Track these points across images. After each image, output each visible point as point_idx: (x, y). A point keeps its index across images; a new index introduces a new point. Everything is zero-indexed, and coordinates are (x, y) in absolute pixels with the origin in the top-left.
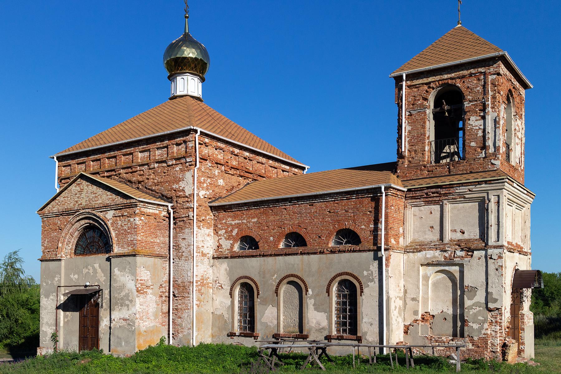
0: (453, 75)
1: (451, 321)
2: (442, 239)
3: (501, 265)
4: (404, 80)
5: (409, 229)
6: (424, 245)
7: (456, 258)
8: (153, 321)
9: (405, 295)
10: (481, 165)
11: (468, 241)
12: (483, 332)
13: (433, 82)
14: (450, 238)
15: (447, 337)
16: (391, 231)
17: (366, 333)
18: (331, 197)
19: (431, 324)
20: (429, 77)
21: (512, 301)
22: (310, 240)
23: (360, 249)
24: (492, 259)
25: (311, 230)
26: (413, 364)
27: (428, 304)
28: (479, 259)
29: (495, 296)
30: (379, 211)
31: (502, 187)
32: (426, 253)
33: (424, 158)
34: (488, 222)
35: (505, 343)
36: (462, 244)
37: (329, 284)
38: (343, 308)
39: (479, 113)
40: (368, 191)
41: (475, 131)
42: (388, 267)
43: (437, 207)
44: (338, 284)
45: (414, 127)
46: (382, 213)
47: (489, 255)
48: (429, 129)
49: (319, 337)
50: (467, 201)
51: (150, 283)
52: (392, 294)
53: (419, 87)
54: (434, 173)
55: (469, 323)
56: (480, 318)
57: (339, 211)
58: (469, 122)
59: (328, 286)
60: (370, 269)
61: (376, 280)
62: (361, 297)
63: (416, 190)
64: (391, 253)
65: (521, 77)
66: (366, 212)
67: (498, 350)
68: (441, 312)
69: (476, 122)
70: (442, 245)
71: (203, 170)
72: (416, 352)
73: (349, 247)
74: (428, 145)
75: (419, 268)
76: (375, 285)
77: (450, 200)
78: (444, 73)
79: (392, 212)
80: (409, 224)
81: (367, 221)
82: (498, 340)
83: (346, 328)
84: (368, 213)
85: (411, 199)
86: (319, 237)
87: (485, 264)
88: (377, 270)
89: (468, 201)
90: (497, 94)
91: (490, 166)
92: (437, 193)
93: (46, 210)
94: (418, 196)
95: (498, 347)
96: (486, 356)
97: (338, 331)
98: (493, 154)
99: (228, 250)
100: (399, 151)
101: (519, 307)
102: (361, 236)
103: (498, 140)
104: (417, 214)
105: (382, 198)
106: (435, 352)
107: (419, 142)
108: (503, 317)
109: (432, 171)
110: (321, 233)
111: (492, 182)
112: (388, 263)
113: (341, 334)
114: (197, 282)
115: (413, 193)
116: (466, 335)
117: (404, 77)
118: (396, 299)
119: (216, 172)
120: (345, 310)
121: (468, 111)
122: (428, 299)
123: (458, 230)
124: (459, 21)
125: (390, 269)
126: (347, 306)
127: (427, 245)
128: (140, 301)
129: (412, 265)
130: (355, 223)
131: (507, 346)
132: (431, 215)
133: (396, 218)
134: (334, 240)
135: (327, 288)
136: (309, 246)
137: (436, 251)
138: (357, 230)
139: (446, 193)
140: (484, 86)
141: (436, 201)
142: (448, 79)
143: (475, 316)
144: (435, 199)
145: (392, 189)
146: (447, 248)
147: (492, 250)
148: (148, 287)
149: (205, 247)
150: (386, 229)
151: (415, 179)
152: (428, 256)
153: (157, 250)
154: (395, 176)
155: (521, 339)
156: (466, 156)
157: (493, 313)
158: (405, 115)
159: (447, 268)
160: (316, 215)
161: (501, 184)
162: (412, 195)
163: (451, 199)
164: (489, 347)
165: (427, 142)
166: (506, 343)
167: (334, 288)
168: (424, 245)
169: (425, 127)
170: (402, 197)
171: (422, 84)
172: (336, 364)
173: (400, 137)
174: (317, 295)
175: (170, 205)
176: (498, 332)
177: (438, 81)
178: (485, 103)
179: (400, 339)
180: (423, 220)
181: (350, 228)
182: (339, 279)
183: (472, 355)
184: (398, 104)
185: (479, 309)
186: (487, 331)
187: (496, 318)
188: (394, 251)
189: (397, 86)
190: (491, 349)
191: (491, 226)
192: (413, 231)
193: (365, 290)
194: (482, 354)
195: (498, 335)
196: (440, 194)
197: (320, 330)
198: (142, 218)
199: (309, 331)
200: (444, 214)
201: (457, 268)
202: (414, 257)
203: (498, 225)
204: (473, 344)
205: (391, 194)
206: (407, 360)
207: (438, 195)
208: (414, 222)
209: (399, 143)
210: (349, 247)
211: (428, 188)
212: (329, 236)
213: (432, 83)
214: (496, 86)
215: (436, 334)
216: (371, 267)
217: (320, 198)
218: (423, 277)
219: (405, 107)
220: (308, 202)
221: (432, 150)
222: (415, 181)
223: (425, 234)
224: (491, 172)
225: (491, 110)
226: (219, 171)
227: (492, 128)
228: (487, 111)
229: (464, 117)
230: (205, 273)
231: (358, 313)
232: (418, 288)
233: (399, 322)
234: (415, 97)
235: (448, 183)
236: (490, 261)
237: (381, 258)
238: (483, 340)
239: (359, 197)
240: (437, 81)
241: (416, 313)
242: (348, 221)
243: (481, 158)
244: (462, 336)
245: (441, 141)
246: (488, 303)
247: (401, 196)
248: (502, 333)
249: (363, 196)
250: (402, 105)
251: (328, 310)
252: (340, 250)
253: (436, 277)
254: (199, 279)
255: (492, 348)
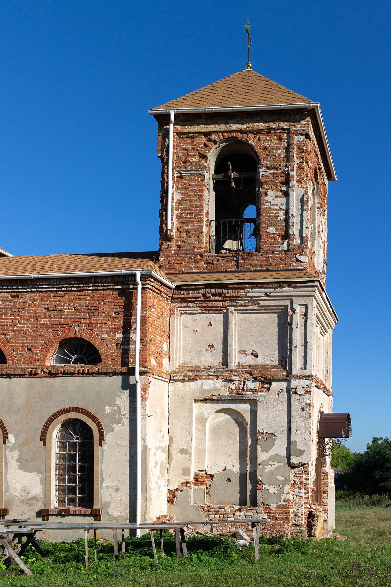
0: (244, 126)
1: (238, 482)
2: (225, 363)
3: (308, 402)
4: (172, 121)
5: (177, 347)
6: (199, 371)
7: (247, 391)
9: (170, 445)
10: (282, 260)
11: (263, 368)
12: (283, 497)
13: (215, 132)
14: (237, 363)
15: (232, 506)
16: (151, 345)
17: (108, 504)
18: (50, 284)
19: (209, 487)
20: (208, 124)
21: (318, 454)
22: (12, 353)
23: (100, 371)
24: (297, 394)
25: (15, 338)
26: (186, 551)
27: (205, 458)
28: (278, 394)
29: (300, 446)
30: (131, 313)
31: (311, 294)
32: (202, 383)
33: (201, 243)
34: (291, 342)
35: (311, 513)
36: (255, 372)
37: (45, 426)
38: (69, 466)
39: (280, 187)
40: (114, 279)
41: (275, 212)
42: (146, 401)
43: (220, 317)
44: (62, 426)
45: (185, 195)
46: (136, 316)
47: (292, 389)
48: (208, 201)
49: (27, 513)
50: (262, 310)
52: (151, 444)
53: (194, 137)
54: (215, 266)
55: (263, 486)
56: (279, 478)
57: (65, 309)
58: (266, 198)
59: (43, 429)
60: (116, 403)
61: (125, 420)
62: (100, 447)
63: (189, 288)
64: (151, 379)
65: (328, 156)
66: (110, 314)
67: (303, 523)
68: (224, 470)
69: (276, 199)
70: (226, 371)
72: (189, 533)
73: (81, 367)
74: (207, 225)
75: (191, 405)
76: (125, 429)
77: (239, 308)
78: (232, 121)
79: (152, 316)
80: (177, 338)
81: (112, 328)
82: (303, 508)
83: (74, 497)
84: (114, 315)
85: (180, 302)
86: (29, 349)
87: (286, 402)
88: (128, 404)
89: (263, 311)
90: (305, 164)
91: (294, 264)
92: (220, 295)
94: (191, 298)
95: (303, 519)
96: (286, 531)
97: (61, 502)
98: (299, 246)
100: (163, 229)
101: (322, 463)
102: (101, 351)
103: (305, 228)
104: (189, 325)
105: (137, 293)
106: (214, 529)
107: (193, 218)
108: (309, 476)
109: (213, 264)
110: (32, 343)
111: (298, 285)
112: (145, 394)
113: (67, 506)
115: (185, 292)
116: (259, 502)
117: (172, 118)
118: (157, 450)
120: (72, 469)
121: (264, 182)
122: (204, 451)
123: (249, 352)
124: (248, 63)
125: (148, 403)
126: (76, 462)
127: (204, 371)
129: (181, 400)
130: (91, 330)
131: (314, 516)
132: (210, 328)
133: (159, 327)
134: (55, 357)
135: (42, 432)
136: (10, 363)
137: (217, 381)
138: (95, 341)
139: (233, 297)
140: (288, 149)
141: (217, 307)
142: (238, 131)
143: (272, 475)
144: (217, 304)
145: (152, 280)
146: (233, 377)
147: (296, 382)
150: (142, 340)
151: (186, 273)
152: (205, 387)
154: (156, 266)
155: (323, 505)
156: (261, 247)
157: (296, 470)
158: (173, 175)
159: (232, 406)
160: (24, 313)
161: (310, 289)
162: (182, 296)
163: (240, 306)
164: (290, 519)
165: (205, 221)
166: (312, 512)
167: (55, 432)
168: (199, 371)
169: (202, 197)
170: (168, 298)
171: (199, 133)
172: (55, 561)
173: (165, 208)
174: (25, 444)
176: (303, 497)
177: (223, 132)
178: (289, 174)
179: (161, 512)
180: (198, 334)
181: (82, 337)
182: (63, 418)
183: (268, 530)
184: (162, 158)
185: (278, 464)
186: (288, 496)
187: (301, 477)
188: (155, 376)
189: (161, 130)
190: (293, 521)
191: (296, 347)
192: (183, 350)
193: (108, 436)
194: (281, 529)
195: (304, 501)
196: (225, 297)
197: (29, 502)
199: (10, 503)
200: (230, 326)
201: (247, 406)
202: (184, 389)
203: (306, 346)
204: (269, 516)
205: (150, 287)
206: (178, 546)
207: (221, 298)
208: (185, 337)
209: (162, 217)
210: (81, 367)
211: (207, 286)
212: (46, 348)
213: (213, 135)
214: (303, 152)
215: (215, 502)
216: (117, 400)
217: (31, 285)
218: (198, 419)
219: (173, 164)
220: (10, 291)
221: (211, 234)
222: (187, 275)
223: (201, 355)
224: (296, 272)
225: (297, 184)
227: (297, 210)
228: (291, 185)
229: (259, 190)
231: (94, 473)
232: (190, 435)
233: (160, 485)
234: (187, 150)
235: (237, 281)
236: (294, 397)
237: (134, 387)
238: (283, 508)
239: (99, 288)
240: (220, 132)
241: (186, 471)
242: (80, 325)
243: (282, 251)
244: (254, 503)
245: (225, 223)
246: (290, 456)
247: (166, 294)
248: (309, 498)
249: (104, 288)
250: (168, 160)
251: (43, 468)
252: (64, 371)
253: (216, 419)
255: (295, 520)
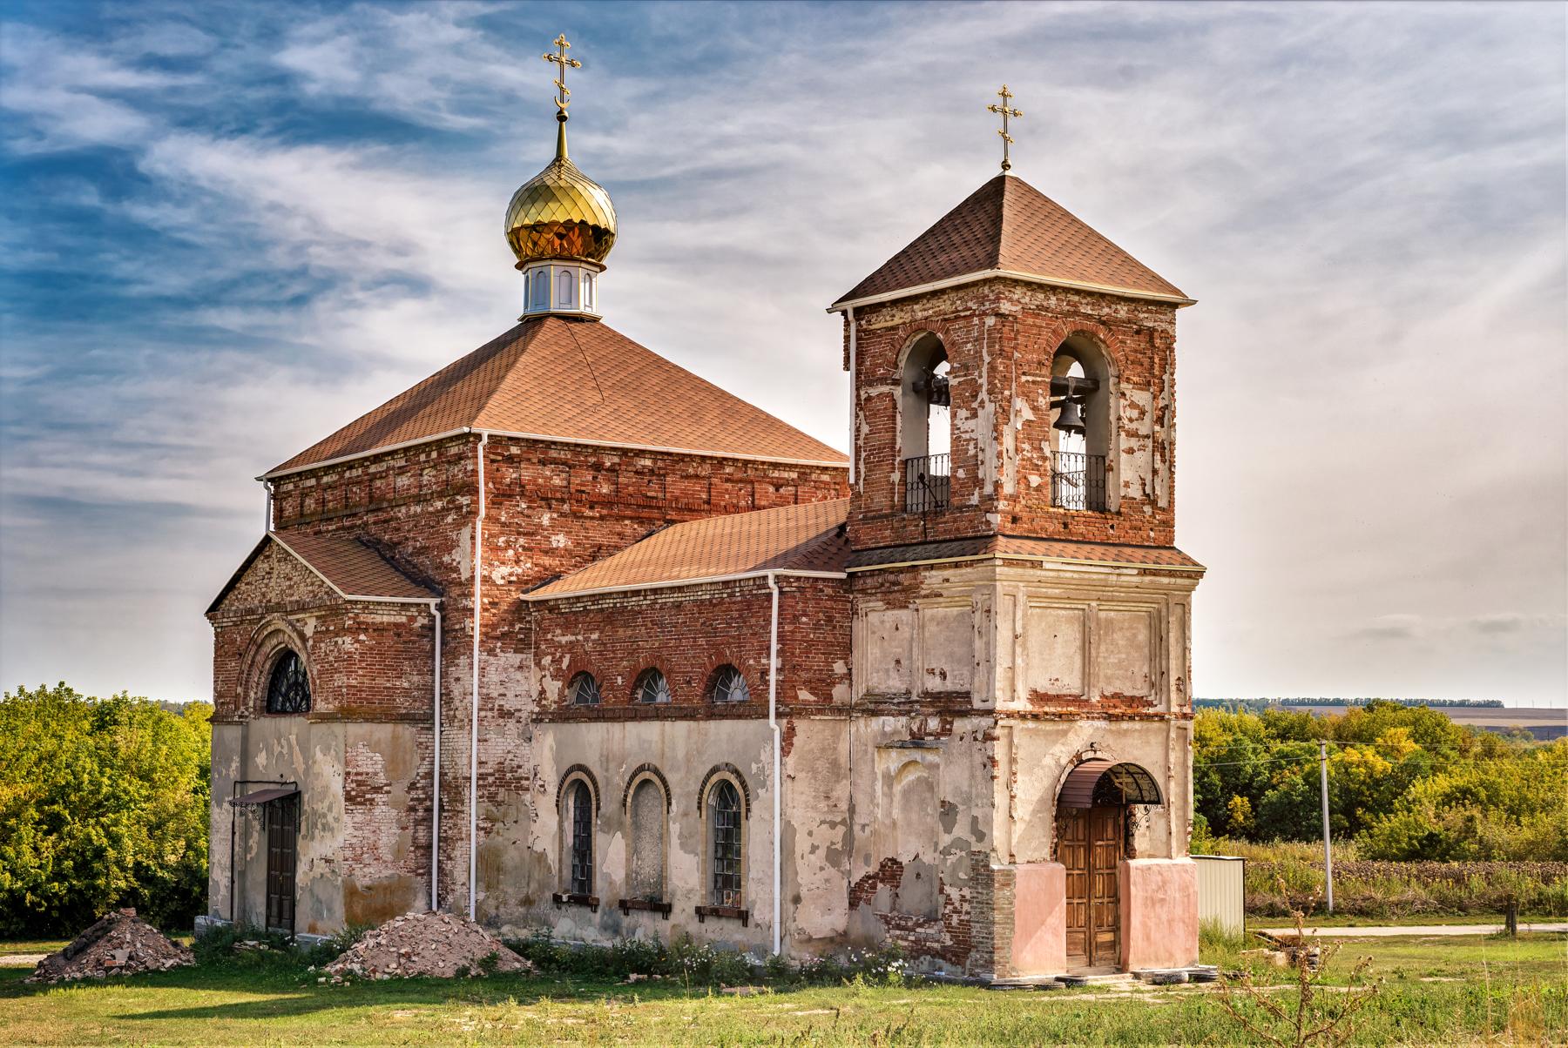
8: (389, 865)
51: (381, 779)
71: (503, 519)
93: (234, 604)
99: (555, 702)
114: (481, 777)
119: (546, 519)
123: (937, 672)
128: (356, 820)
132: (897, 633)
148: (377, 790)
149: (510, 695)
153: (403, 704)
175: (433, 602)
193: (754, 806)
198: (362, 637)
226: (555, 515)
230: (510, 756)
254: (492, 771)
